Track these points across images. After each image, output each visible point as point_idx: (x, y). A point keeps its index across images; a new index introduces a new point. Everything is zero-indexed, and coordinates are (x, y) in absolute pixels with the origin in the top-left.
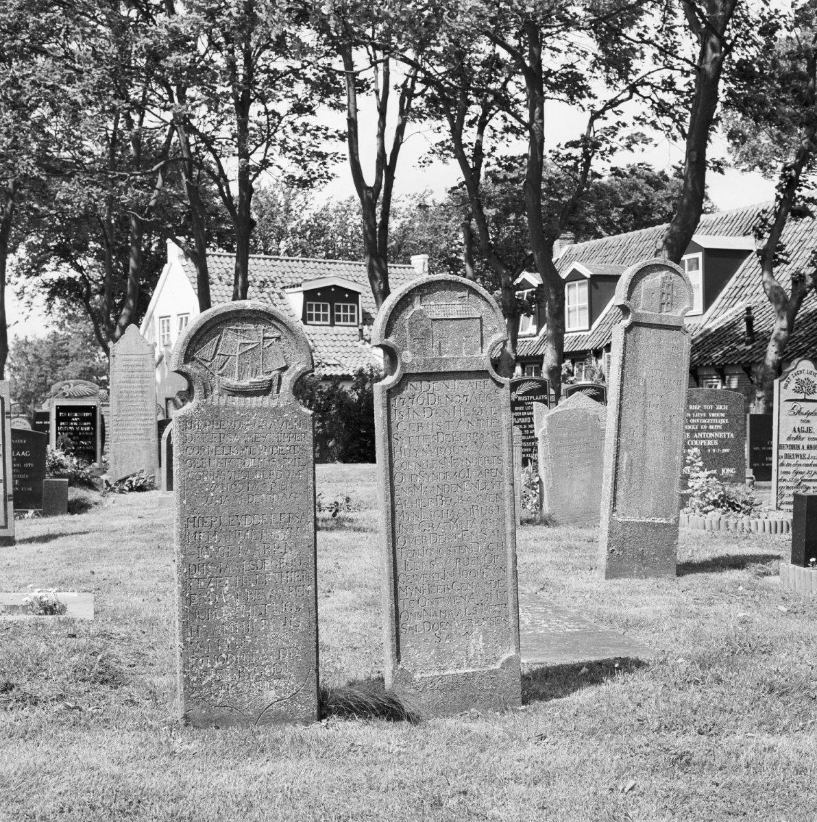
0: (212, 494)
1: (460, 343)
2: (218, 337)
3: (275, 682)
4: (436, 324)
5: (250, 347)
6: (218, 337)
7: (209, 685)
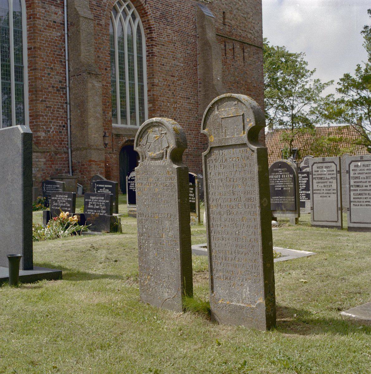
0: (145, 203)
1: (234, 129)
2: (147, 135)
4: (223, 120)
6: (147, 135)
7: (147, 285)
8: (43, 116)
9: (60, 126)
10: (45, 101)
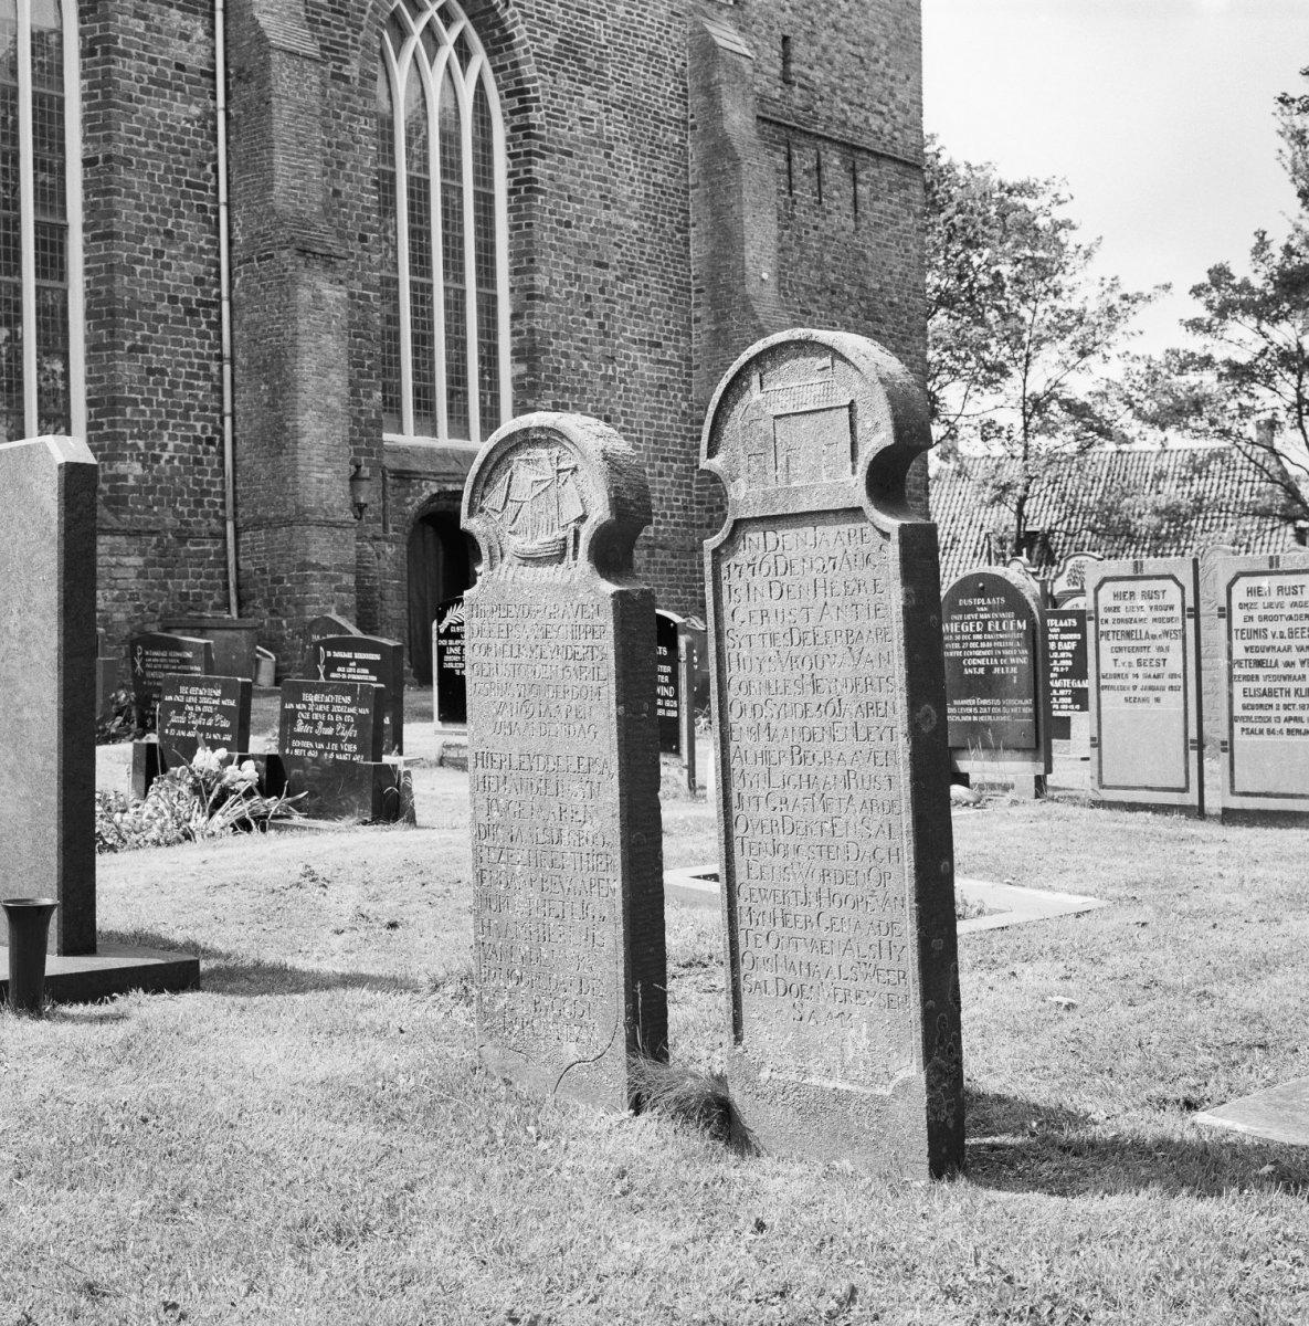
3: (576, 1029)
5: (543, 486)
8: (134, 402)
9: (197, 440)
10: (144, 350)
